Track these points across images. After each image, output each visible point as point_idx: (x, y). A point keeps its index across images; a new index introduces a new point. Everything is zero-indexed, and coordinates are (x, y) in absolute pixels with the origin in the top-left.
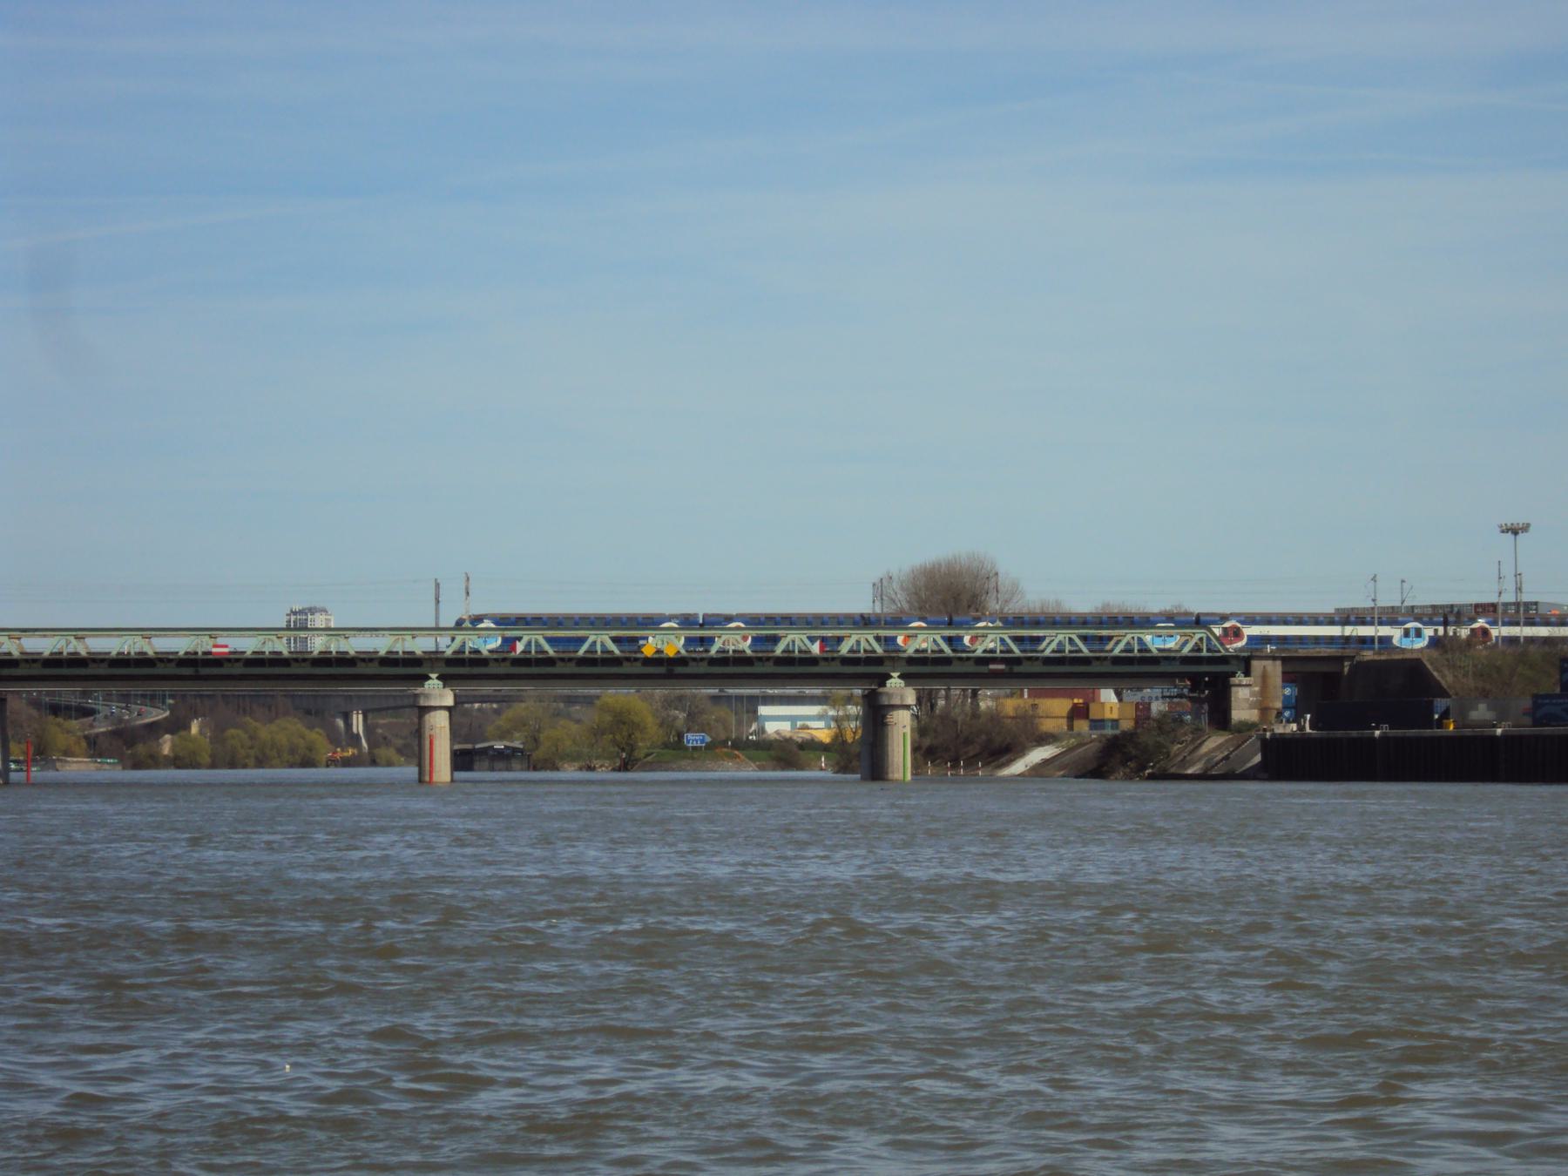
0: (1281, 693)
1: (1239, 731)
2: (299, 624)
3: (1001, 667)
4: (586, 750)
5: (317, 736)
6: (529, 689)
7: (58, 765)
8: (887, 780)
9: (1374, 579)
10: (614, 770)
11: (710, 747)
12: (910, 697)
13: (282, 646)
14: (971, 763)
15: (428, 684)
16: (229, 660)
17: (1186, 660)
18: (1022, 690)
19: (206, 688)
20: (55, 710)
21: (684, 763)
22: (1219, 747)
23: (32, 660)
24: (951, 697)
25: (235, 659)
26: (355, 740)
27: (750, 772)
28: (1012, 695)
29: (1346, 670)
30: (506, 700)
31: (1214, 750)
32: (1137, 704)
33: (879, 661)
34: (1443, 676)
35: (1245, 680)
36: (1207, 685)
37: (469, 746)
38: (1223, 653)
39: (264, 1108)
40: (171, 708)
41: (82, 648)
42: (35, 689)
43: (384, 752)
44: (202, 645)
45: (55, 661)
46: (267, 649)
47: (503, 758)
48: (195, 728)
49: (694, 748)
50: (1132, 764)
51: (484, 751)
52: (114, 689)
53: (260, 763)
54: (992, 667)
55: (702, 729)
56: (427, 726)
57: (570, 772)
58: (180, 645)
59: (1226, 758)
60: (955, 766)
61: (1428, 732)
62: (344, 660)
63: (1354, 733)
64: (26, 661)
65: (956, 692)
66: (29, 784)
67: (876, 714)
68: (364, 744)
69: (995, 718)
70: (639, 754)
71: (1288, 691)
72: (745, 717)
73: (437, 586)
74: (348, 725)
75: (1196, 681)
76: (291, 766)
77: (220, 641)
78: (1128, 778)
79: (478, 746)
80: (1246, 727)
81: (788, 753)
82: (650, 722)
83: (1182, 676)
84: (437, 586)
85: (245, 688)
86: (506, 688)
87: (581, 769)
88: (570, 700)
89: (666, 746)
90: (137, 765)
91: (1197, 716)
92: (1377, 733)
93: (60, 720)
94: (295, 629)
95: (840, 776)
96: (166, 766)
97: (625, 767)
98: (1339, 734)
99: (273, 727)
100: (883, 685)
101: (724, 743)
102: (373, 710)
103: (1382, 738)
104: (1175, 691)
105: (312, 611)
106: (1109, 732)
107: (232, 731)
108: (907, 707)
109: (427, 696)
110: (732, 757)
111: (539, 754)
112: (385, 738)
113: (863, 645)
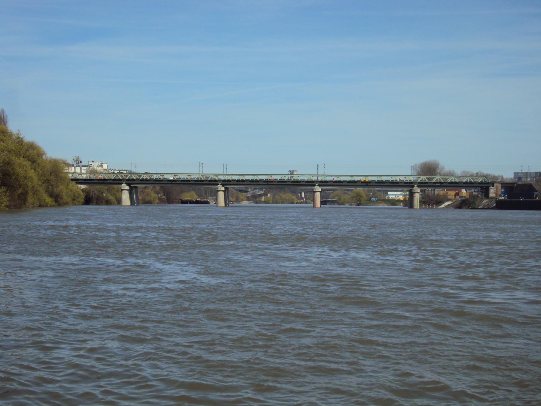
0: (500, 190)
1: (491, 199)
2: (291, 173)
3: (439, 184)
4: (350, 201)
5: (294, 197)
6: (337, 188)
7: (241, 203)
8: (414, 208)
9: (522, 166)
10: (356, 205)
11: (377, 201)
12: (419, 191)
13: (286, 178)
14: (432, 205)
15: (219, 186)
16: (274, 181)
17: (480, 183)
18: (444, 190)
19: (272, 187)
20: (240, 191)
21: (372, 204)
22: (486, 202)
23: (234, 180)
24: (429, 191)
25: (275, 181)
26: (302, 198)
27: (386, 206)
28: (443, 190)
29: (515, 186)
30: (334, 190)
31: (485, 203)
32: (470, 193)
33: (121, 180)
34: (537, 188)
35: (493, 188)
36: (484, 189)
37: (326, 200)
38: (488, 182)
39: (361, 265)
40: (264, 191)
41: (244, 178)
42: (236, 187)
43: (309, 201)
44: (269, 178)
45: (238, 181)
46: (380, 180)
47: (333, 202)
48: (269, 195)
49: (374, 201)
50: (467, 206)
51: (329, 201)
52: (253, 187)
53: (282, 203)
54: (437, 184)
55: (376, 197)
56: (315, 195)
57: (347, 206)
58: (264, 178)
59: (488, 204)
60: (429, 206)
61: (532, 200)
62: (298, 181)
63: (516, 199)
64: (401, 182)
65: (430, 189)
66: (233, 206)
67: (412, 194)
68: (304, 199)
69: (438, 195)
70: (362, 202)
71: (503, 190)
72: (385, 194)
73: (318, 166)
74: (301, 195)
75: (482, 188)
76: (289, 203)
77: (272, 177)
78: (466, 209)
79: (328, 200)
80: (493, 198)
81: (394, 202)
82: (364, 195)
83: (479, 187)
84: (318, 166)
85: (278, 187)
86: (332, 188)
87: (349, 205)
88: (348, 190)
89: (368, 200)
90: (257, 203)
91: (482, 195)
92: (521, 199)
93: (241, 193)
94: (290, 175)
95: (404, 207)
96: (263, 203)
97: (359, 205)
98: (513, 200)
99: (285, 195)
100: (413, 188)
101: (380, 200)
102: (306, 192)
103: (522, 201)
104: (477, 190)
105: (294, 171)
106: (463, 198)
107: (277, 196)
108: (418, 193)
109: (315, 189)
110: (381, 203)
111: (340, 202)
112: (309, 198)
113: (423, 180)
